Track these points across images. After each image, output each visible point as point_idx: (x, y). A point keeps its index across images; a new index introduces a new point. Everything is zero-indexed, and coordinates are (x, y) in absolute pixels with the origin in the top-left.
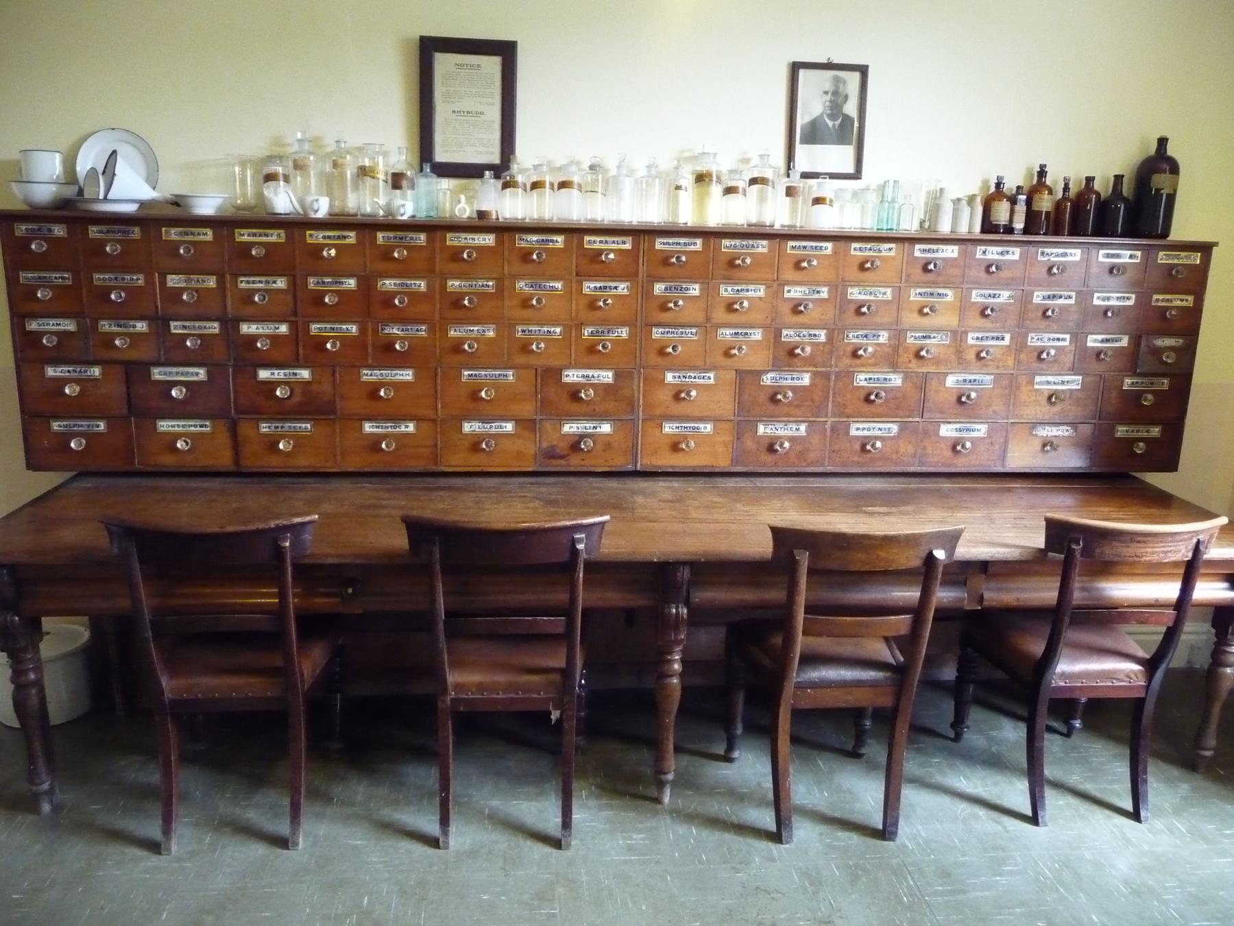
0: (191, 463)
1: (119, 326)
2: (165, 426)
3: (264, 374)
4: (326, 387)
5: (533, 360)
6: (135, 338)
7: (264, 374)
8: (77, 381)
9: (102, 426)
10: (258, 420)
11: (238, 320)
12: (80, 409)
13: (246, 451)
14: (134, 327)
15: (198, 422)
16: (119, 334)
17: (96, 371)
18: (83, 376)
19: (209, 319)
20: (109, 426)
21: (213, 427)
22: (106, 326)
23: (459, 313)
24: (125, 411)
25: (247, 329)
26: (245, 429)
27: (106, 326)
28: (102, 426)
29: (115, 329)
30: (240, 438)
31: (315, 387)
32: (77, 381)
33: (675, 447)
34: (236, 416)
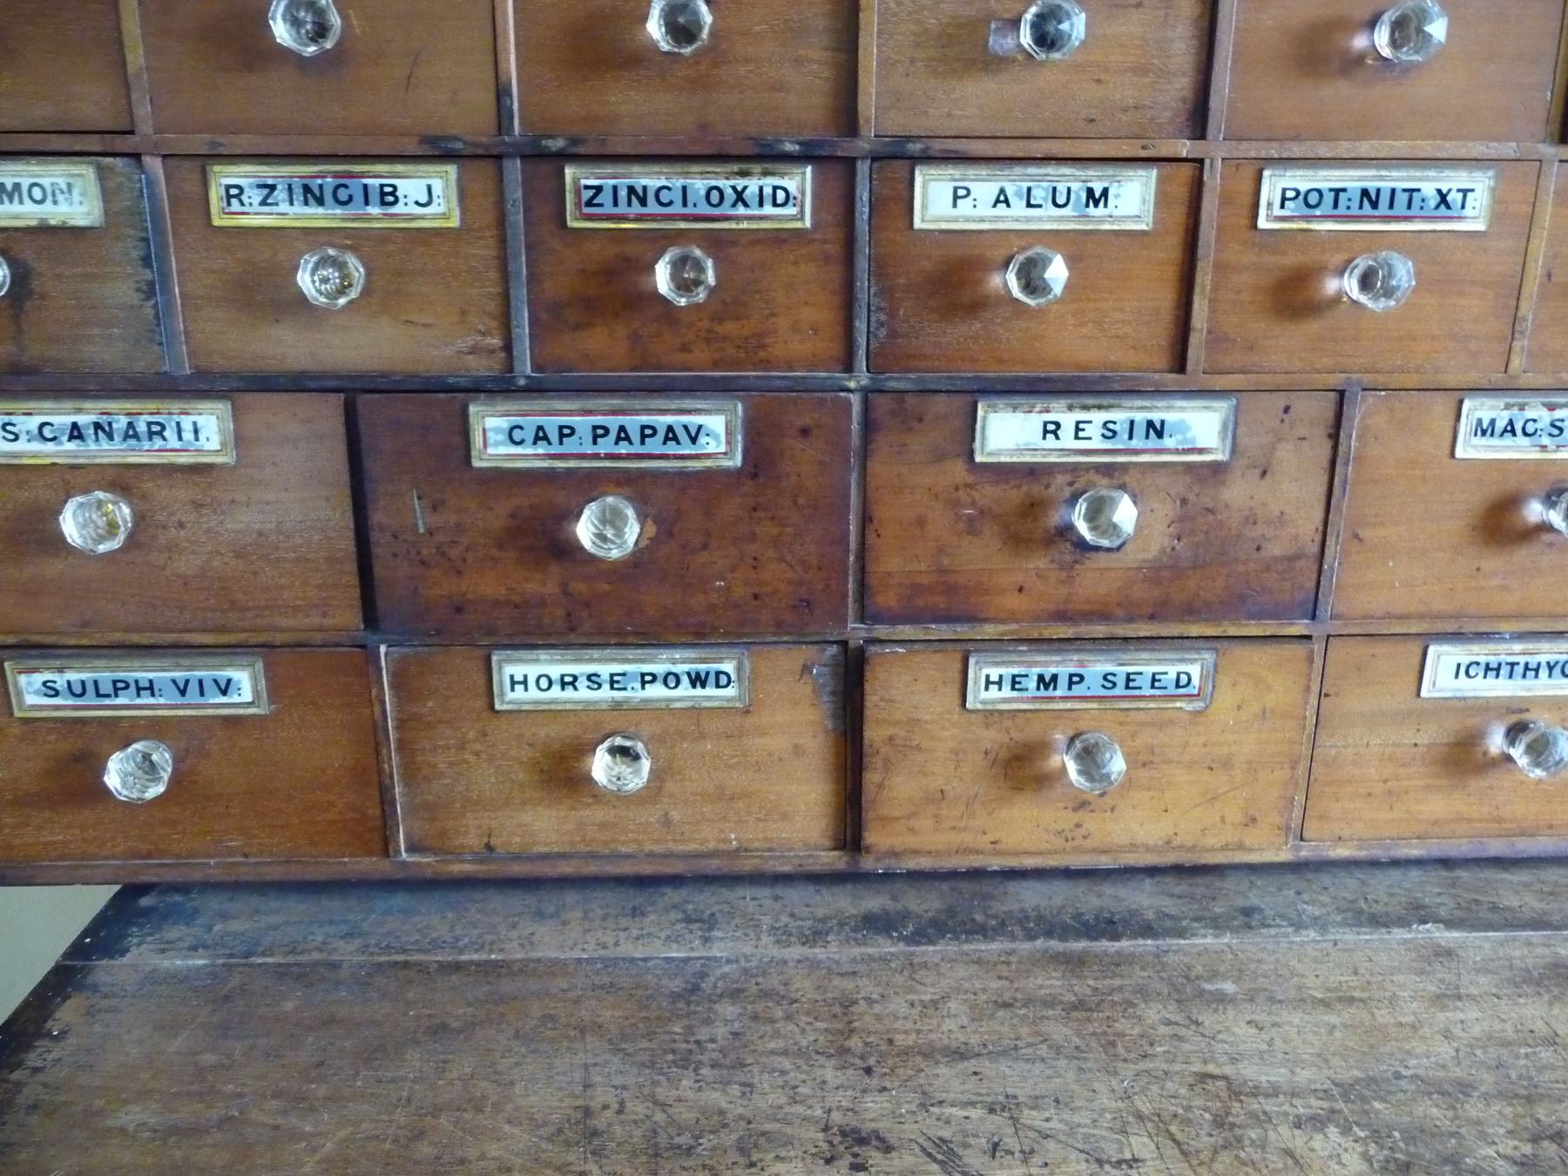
0: (641, 841)
1: (312, 195)
2: (531, 679)
3: (1008, 432)
4: (1289, 496)
5: (289, 347)
6: (397, 257)
7: (1008, 432)
8: (636, 485)
9: (244, 685)
10: (965, 651)
11: (903, 156)
12: (146, 614)
13: (894, 790)
14: (388, 197)
15: (679, 662)
16: (313, 237)
17: (205, 430)
18: (144, 454)
19: (768, 156)
20: (275, 687)
21: (752, 682)
22: (248, 199)
23: (1337, 93)
24: (348, 617)
25: (941, 201)
26: (903, 691)
27: (248, 199)
28: (244, 685)
29: (294, 213)
30: (873, 734)
31: (1238, 493)
32: (122, 480)
33: (1462, 757)
34: (370, 638)
